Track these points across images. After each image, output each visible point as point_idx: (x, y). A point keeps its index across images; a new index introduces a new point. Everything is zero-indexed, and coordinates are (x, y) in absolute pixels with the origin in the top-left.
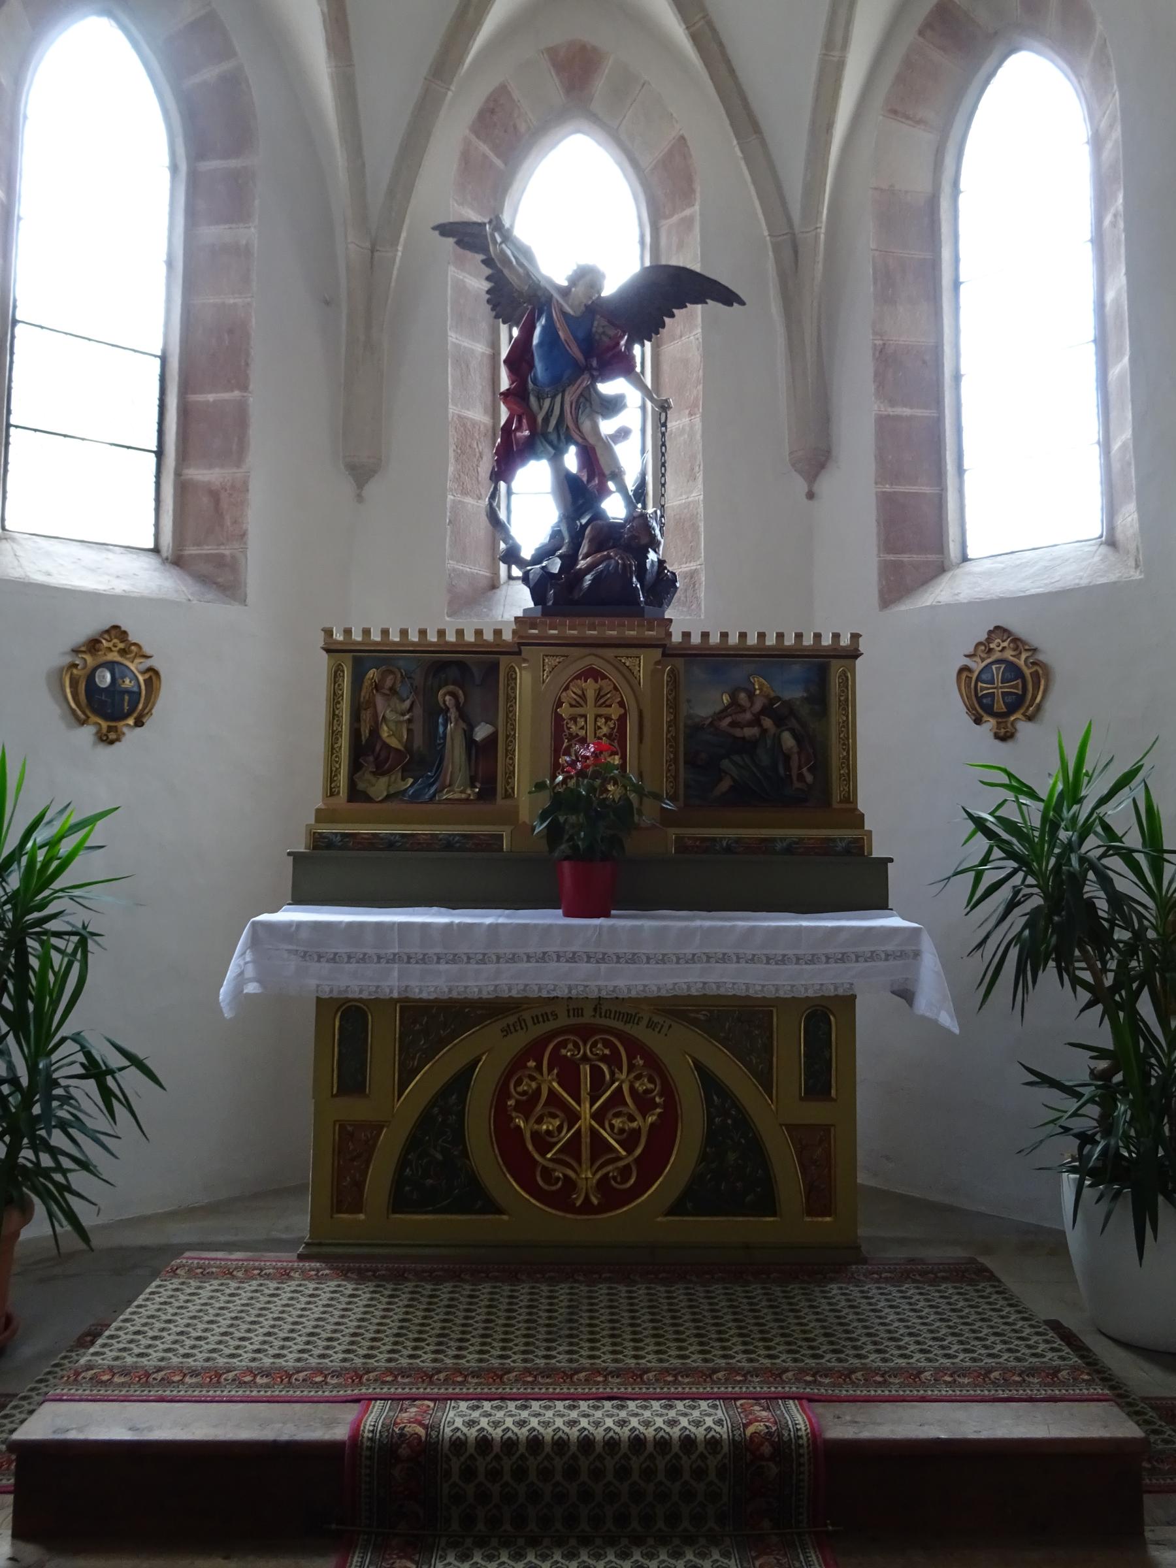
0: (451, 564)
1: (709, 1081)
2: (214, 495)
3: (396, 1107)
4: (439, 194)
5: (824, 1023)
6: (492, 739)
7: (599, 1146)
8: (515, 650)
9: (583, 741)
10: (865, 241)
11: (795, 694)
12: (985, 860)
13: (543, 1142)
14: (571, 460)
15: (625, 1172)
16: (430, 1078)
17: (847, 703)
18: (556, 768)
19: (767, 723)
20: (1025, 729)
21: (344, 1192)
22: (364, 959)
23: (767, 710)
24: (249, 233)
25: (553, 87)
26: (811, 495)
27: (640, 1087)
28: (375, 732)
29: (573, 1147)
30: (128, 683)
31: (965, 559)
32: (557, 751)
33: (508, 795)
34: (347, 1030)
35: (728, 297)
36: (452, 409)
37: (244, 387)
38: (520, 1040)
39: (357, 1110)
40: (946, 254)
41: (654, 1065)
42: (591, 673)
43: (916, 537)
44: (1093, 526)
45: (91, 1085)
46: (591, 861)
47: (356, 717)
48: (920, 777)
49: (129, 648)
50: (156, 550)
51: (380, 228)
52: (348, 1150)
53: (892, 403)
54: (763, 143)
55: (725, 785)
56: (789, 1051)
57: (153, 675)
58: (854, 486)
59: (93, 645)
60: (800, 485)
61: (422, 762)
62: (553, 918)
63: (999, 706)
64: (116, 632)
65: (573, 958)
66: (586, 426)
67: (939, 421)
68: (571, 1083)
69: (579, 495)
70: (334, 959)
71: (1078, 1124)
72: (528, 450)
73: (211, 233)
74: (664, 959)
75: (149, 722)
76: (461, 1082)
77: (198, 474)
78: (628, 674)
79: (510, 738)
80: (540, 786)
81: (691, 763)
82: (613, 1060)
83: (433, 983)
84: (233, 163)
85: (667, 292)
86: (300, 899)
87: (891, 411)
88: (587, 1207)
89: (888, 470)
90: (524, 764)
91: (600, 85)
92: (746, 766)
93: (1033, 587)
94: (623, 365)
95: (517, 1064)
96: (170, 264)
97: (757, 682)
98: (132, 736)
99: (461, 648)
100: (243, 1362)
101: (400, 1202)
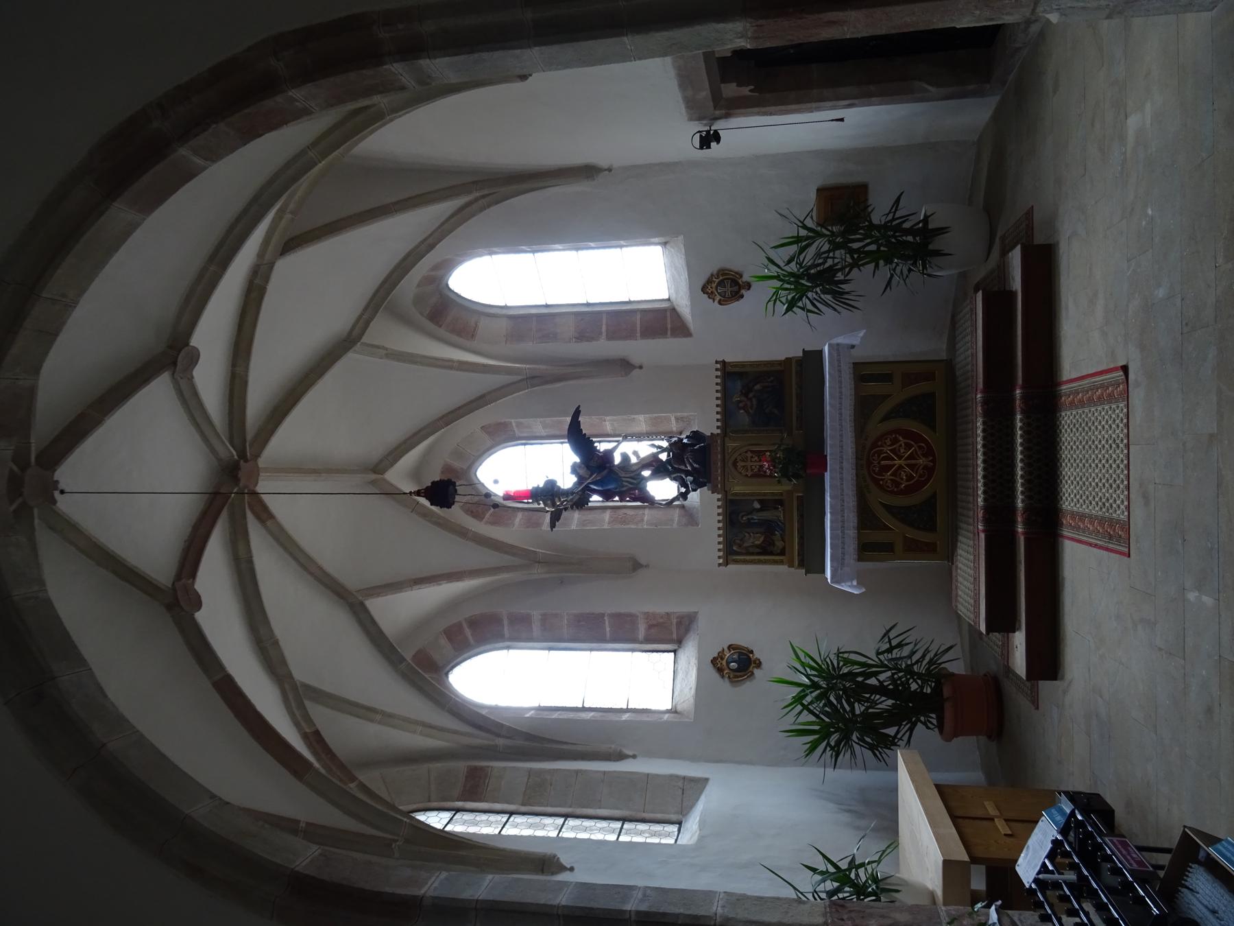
0: (675, 525)
1: (886, 418)
2: (650, 627)
4: (512, 533)
5: (867, 375)
6: (760, 501)
7: (911, 457)
8: (726, 493)
9: (762, 466)
10: (529, 347)
12: (803, 309)
13: (910, 478)
14: (646, 473)
15: (920, 447)
18: (771, 476)
19: (751, 395)
20: (746, 278)
21: (926, 550)
22: (843, 543)
23: (746, 395)
24: (536, 615)
26: (641, 367)
27: (889, 443)
28: (757, 546)
29: (911, 466)
30: (735, 656)
31: (669, 300)
32: (765, 476)
33: (781, 494)
34: (870, 547)
35: (577, 413)
36: (606, 527)
37: (603, 615)
40: (534, 311)
42: (735, 464)
43: (657, 321)
44: (659, 249)
45: (895, 651)
46: (806, 462)
47: (752, 554)
48: (765, 331)
49: (721, 655)
50: (675, 651)
51: (530, 559)
52: (914, 549)
53: (601, 333)
54: (489, 393)
55: (776, 411)
56: (874, 388)
57: (730, 647)
58: (638, 349)
59: (720, 671)
60: (636, 372)
61: (769, 528)
62: (827, 476)
63: (736, 288)
64: (714, 661)
65: (842, 468)
66: (635, 468)
67: (608, 313)
69: (660, 470)
70: (843, 554)
71: (905, 272)
73: (536, 629)
74: (841, 436)
75: (751, 648)
76: (886, 507)
79: (759, 494)
80: (779, 482)
82: (880, 452)
83: (852, 519)
84: (506, 622)
85: (579, 439)
86: (823, 571)
87: (604, 334)
88: (933, 461)
89: (629, 335)
90: (770, 489)
91: (457, 464)
92: (766, 399)
93: (685, 275)
94: (608, 455)
96: (550, 649)
97: (736, 399)
98: (757, 655)
99: (725, 514)
100: (972, 572)
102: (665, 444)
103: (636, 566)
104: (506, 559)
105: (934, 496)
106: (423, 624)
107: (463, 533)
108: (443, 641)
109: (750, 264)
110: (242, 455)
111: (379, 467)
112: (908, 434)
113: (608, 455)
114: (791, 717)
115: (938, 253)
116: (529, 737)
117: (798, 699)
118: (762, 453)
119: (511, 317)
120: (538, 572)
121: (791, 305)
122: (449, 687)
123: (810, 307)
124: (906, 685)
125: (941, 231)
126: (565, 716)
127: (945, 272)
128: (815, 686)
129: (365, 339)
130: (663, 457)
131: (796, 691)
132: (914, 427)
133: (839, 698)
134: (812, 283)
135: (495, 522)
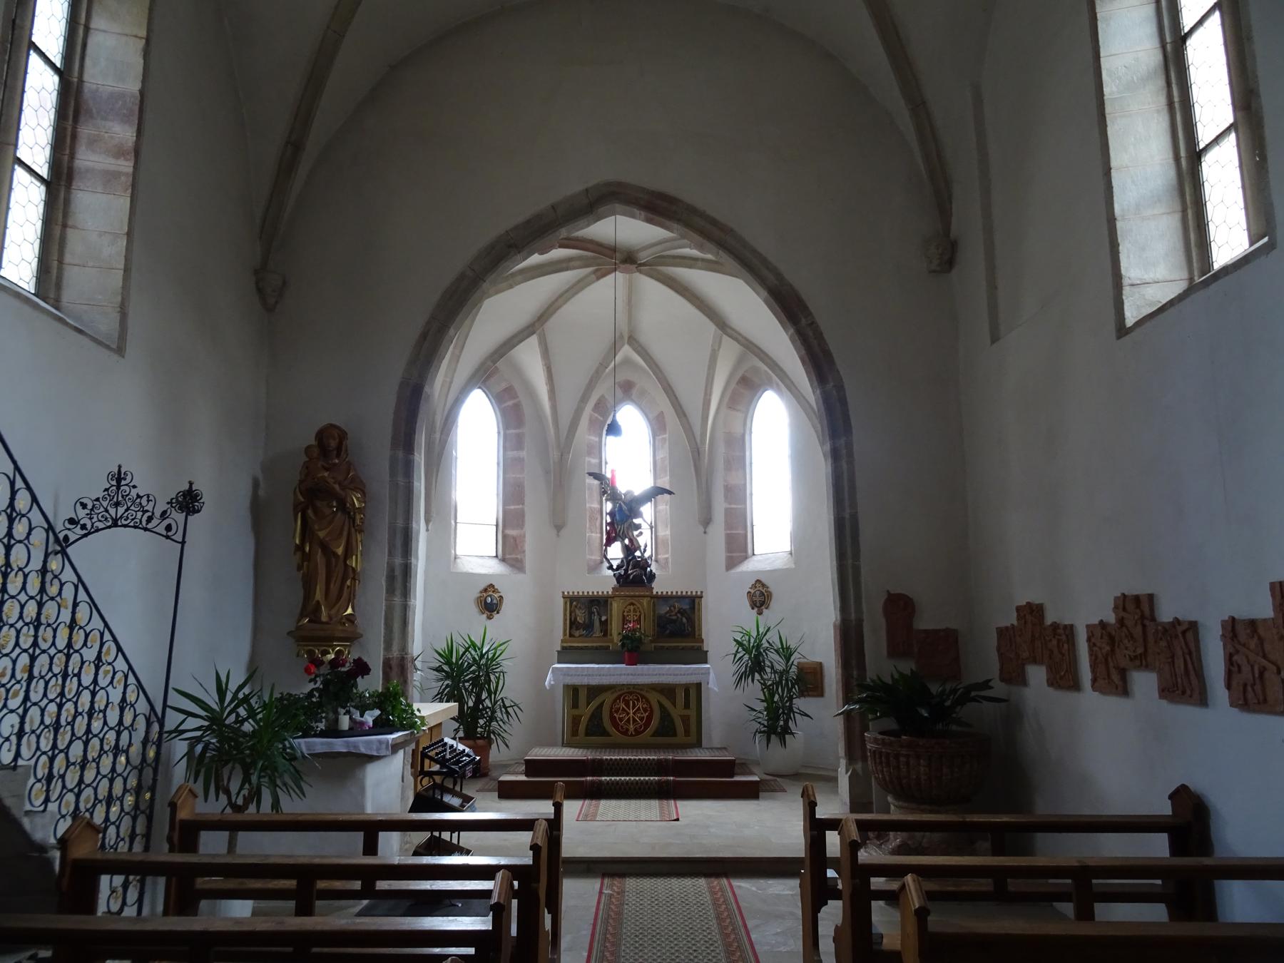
1: (661, 705)
2: (515, 538)
3: (586, 711)
5: (693, 692)
7: (634, 721)
10: (721, 450)
11: (686, 607)
13: (621, 720)
14: (627, 541)
16: (594, 705)
17: (700, 610)
21: (574, 732)
24: (523, 454)
25: (619, 393)
29: (628, 721)
38: (615, 695)
39: (576, 712)
41: (648, 701)
42: (632, 604)
43: (738, 547)
44: (789, 549)
46: (633, 652)
48: (724, 624)
49: (495, 591)
52: (575, 721)
58: (718, 530)
59: (485, 590)
61: (588, 626)
64: (492, 586)
68: (627, 705)
69: (629, 550)
72: (614, 540)
73: (511, 454)
76: (601, 705)
77: (510, 532)
78: (642, 604)
81: (659, 625)
83: (595, 681)
86: (559, 662)
89: (728, 526)
91: (634, 392)
95: (615, 701)
98: (496, 616)
101: (587, 734)
102: (647, 555)
103: (559, 528)
104: (564, 433)
105: (609, 735)
106: (518, 371)
107: (584, 399)
108: (504, 385)
109: (771, 616)
110: (641, 265)
111: (633, 340)
112: (649, 719)
113: (639, 515)
114: (460, 641)
115: (769, 740)
116: (441, 455)
117: (473, 645)
118: (640, 620)
119: (743, 435)
120: (554, 454)
121: (739, 643)
122: (470, 390)
123: (739, 656)
124: (482, 717)
125: (783, 742)
126: (18, 102)
127: (757, 747)
128: (482, 656)
129: (725, 338)
130: (638, 554)
131: (479, 644)
132: (655, 722)
133: (473, 672)
134: (754, 659)
135: (592, 422)
